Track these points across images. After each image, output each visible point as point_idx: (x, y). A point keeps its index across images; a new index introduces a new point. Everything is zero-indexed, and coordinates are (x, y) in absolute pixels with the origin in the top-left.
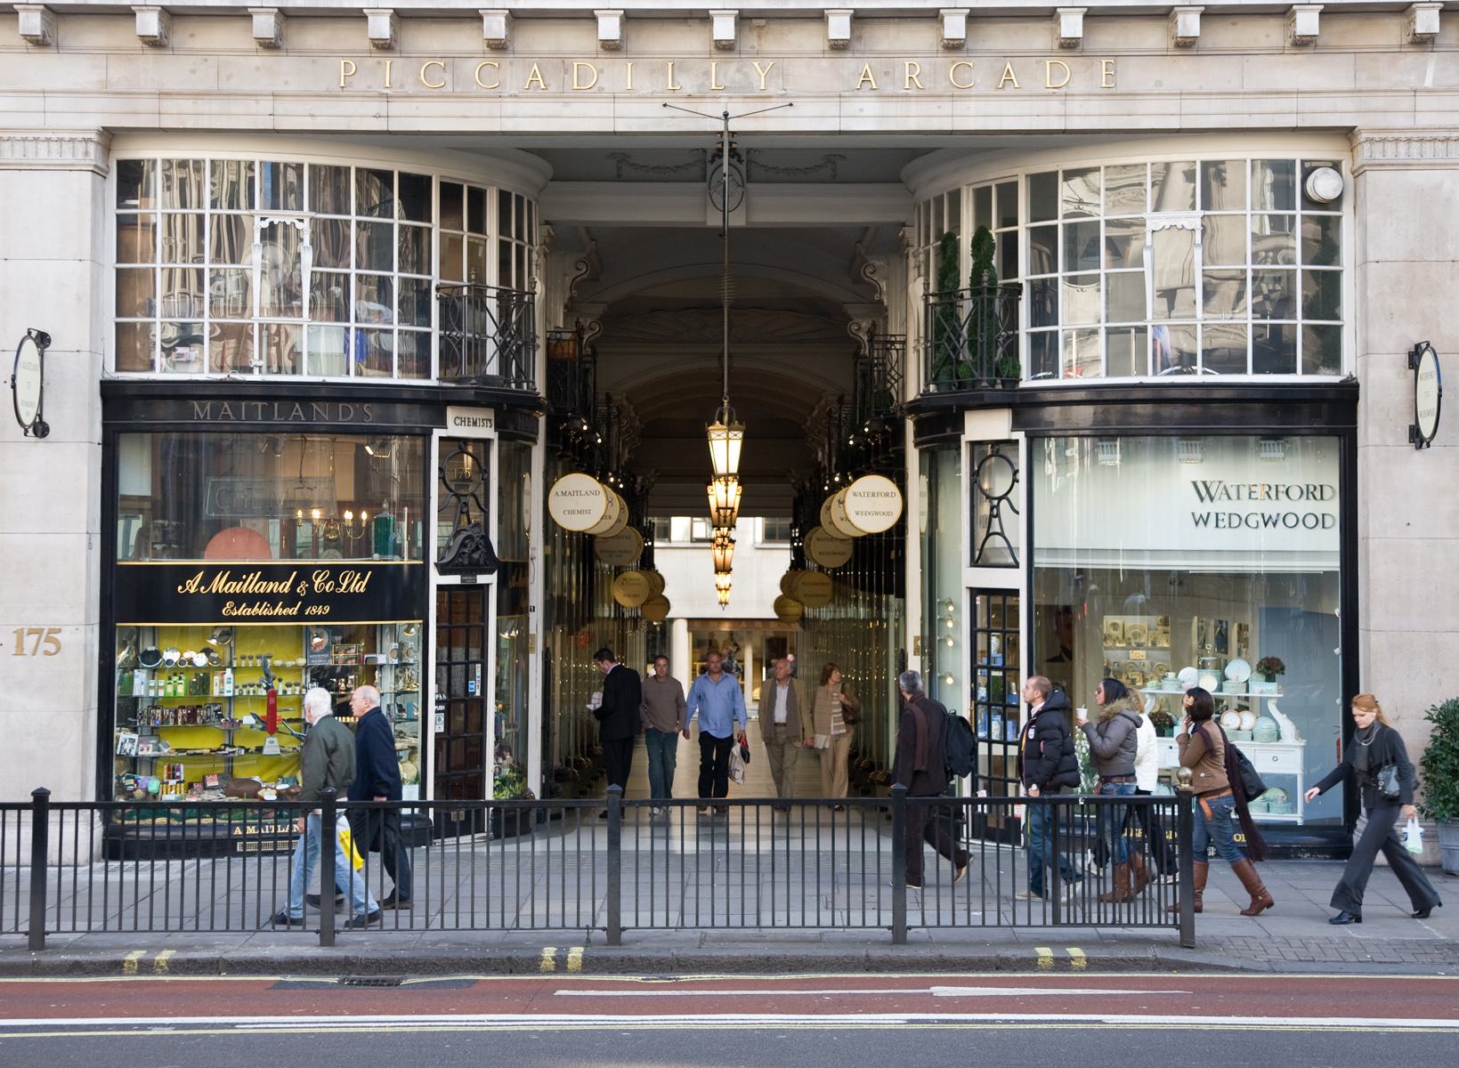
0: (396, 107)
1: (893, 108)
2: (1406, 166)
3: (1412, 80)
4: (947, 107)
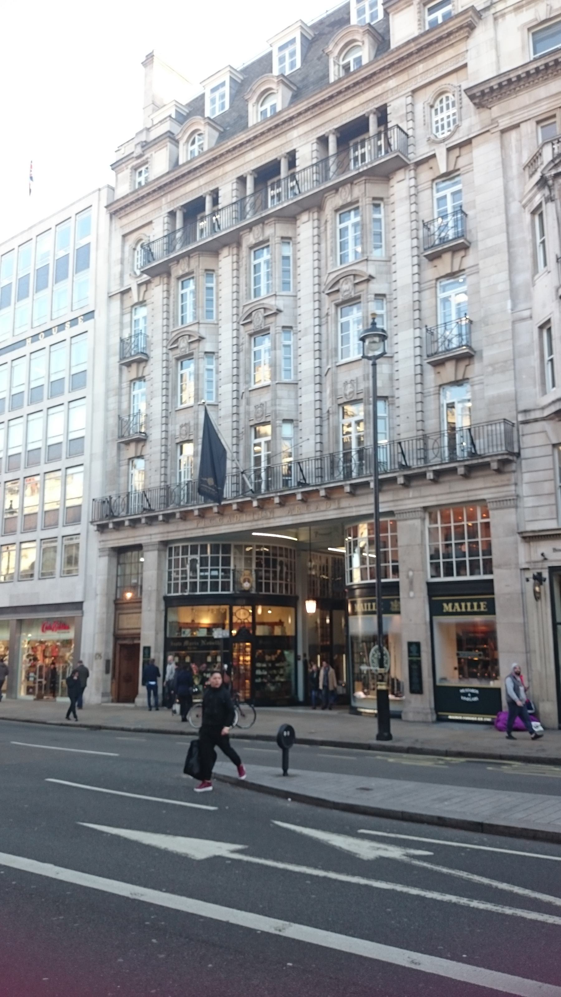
0: (206, 530)
1: (295, 517)
2: (406, 520)
3: (406, 496)
4: (298, 517)
